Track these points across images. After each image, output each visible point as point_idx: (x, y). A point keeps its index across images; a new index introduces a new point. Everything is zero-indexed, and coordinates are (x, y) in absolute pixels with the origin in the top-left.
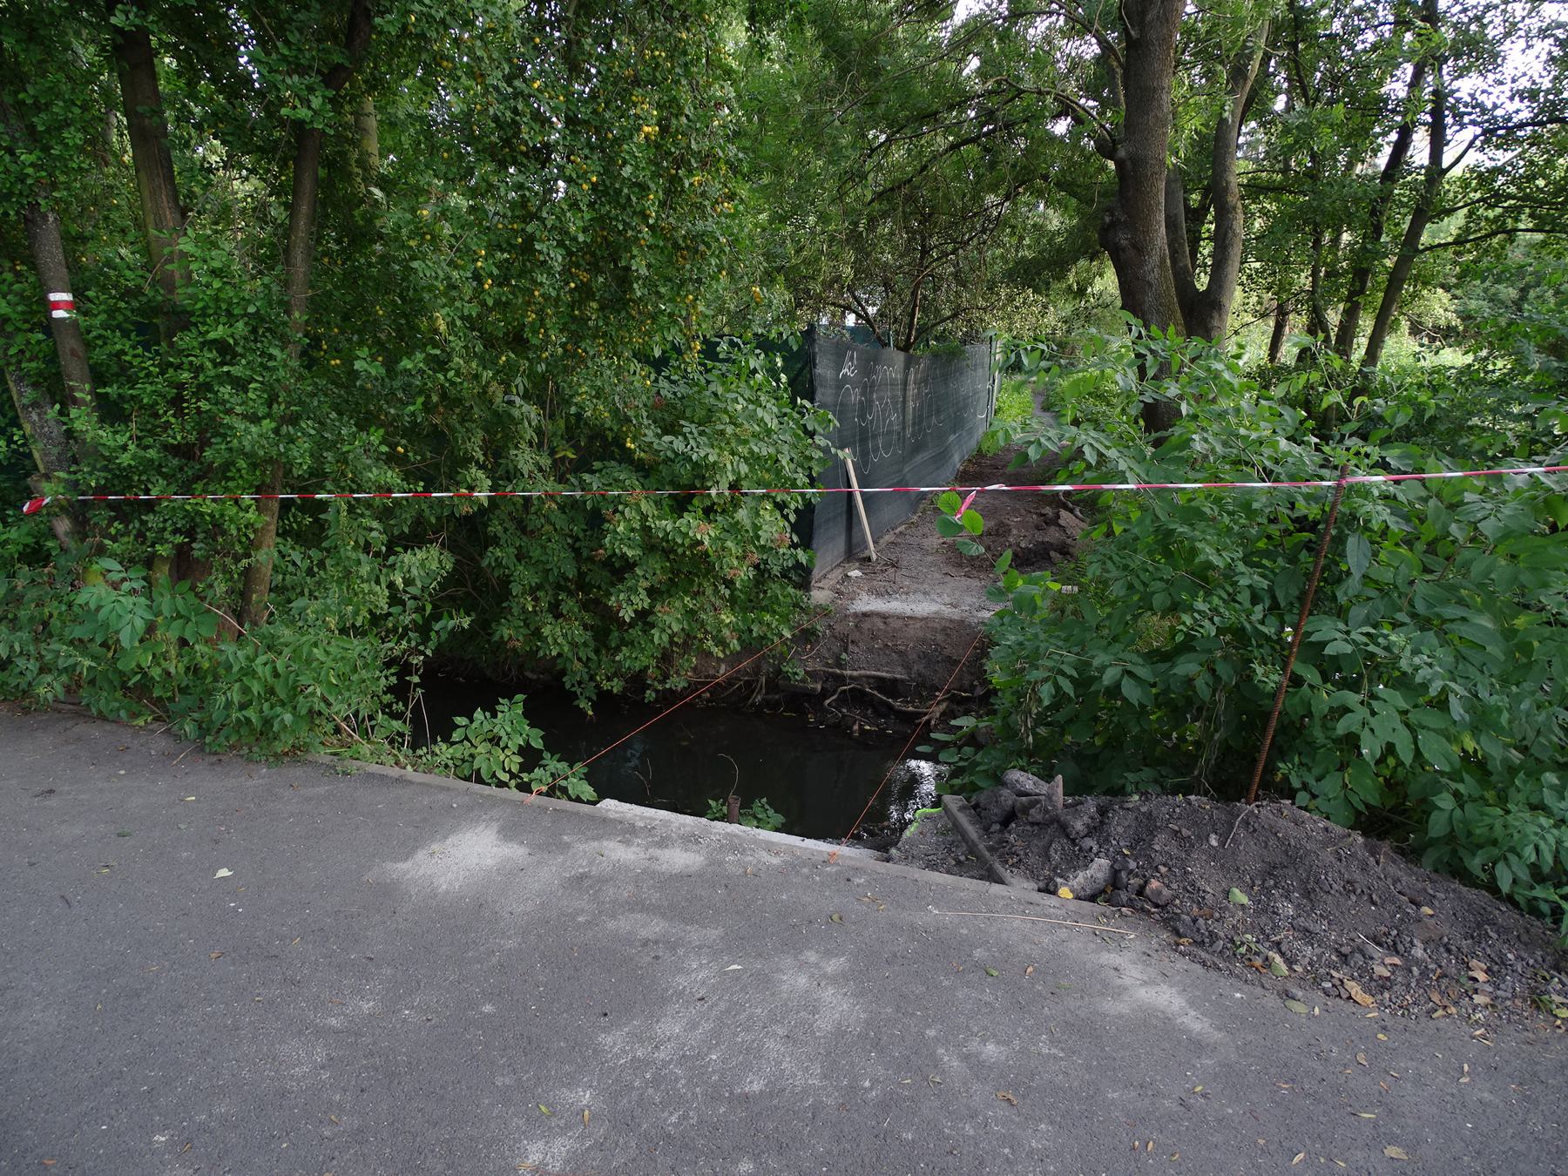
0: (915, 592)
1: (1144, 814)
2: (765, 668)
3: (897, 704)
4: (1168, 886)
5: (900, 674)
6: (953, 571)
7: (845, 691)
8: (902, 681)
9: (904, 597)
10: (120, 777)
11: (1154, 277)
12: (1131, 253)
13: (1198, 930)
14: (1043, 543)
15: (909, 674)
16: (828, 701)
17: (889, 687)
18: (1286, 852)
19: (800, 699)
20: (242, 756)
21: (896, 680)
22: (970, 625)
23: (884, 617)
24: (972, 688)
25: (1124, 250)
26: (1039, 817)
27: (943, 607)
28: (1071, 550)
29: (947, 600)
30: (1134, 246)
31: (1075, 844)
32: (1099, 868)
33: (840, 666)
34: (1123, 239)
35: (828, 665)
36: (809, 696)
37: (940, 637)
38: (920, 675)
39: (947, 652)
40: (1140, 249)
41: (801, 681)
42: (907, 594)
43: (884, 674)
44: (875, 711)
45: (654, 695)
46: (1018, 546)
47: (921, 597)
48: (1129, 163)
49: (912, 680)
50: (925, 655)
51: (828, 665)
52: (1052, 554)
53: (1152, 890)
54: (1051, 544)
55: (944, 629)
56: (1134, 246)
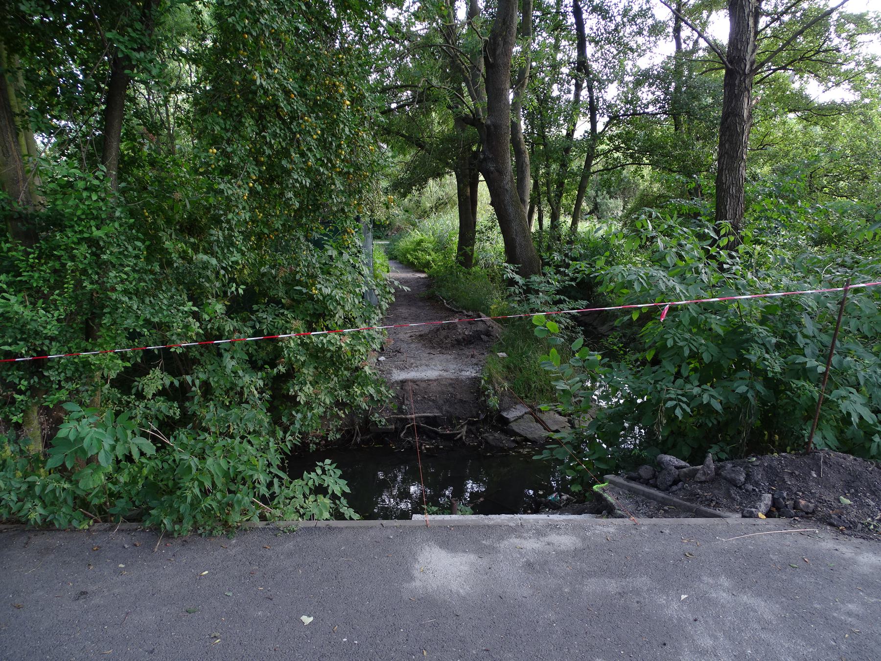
0: (421, 366)
1: (767, 466)
2: (357, 420)
3: (439, 430)
4: (810, 502)
5: (437, 413)
6: (432, 351)
7: (409, 427)
8: (439, 417)
9: (416, 369)
10: (119, 572)
11: (508, 187)
12: (496, 174)
13: (844, 521)
14: (477, 331)
15: (441, 412)
16: (402, 435)
17: (432, 421)
18: (850, 474)
19: (382, 436)
20: (201, 535)
21: (435, 417)
22: (462, 380)
23: (414, 381)
24: (478, 416)
25: (492, 173)
26: (703, 478)
27: (441, 373)
28: (492, 334)
29: (441, 368)
30: (498, 171)
31: (741, 489)
32: (767, 498)
33: (402, 413)
34: (491, 167)
35: (394, 413)
36: (386, 433)
37: (451, 389)
38: (448, 412)
39: (458, 396)
40: (501, 172)
41: (385, 425)
42: (417, 367)
43: (429, 414)
44: (428, 436)
45: (315, 446)
46: (464, 334)
47: (425, 368)
48: (492, 127)
49: (444, 415)
50: (447, 400)
51: (394, 413)
52: (482, 336)
53: (803, 506)
54: (481, 331)
55: (450, 384)
56: (498, 171)
